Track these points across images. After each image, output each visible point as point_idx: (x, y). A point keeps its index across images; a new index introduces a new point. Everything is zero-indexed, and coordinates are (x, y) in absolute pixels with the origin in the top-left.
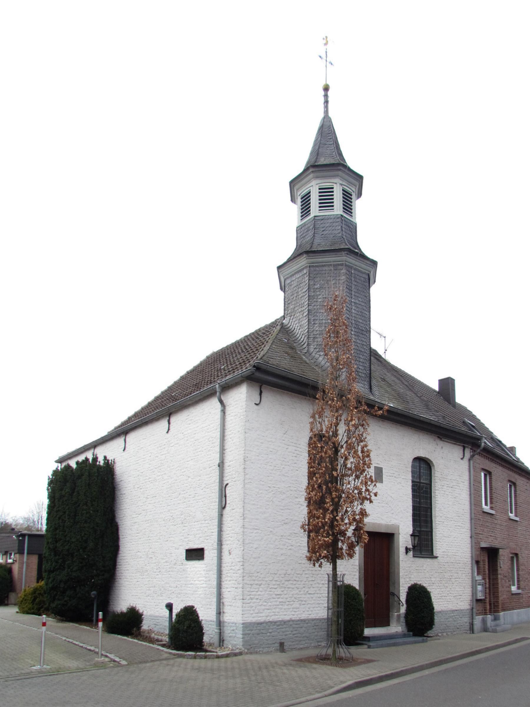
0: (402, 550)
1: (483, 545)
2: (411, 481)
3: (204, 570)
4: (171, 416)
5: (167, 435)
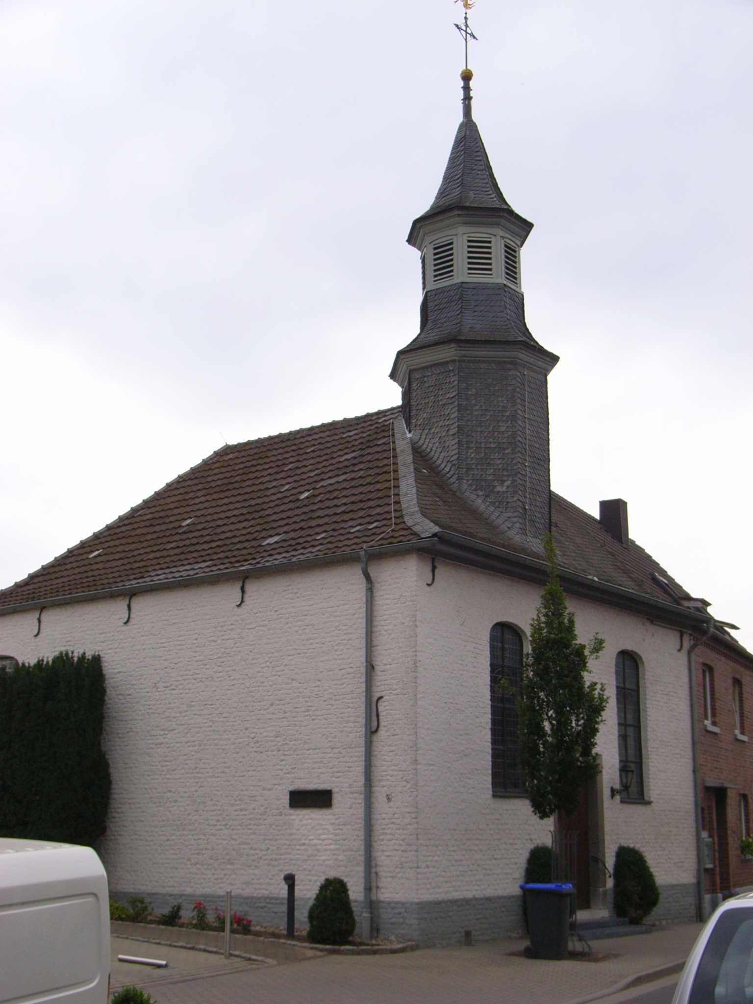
0: (606, 792)
1: (708, 784)
2: (614, 688)
3: (333, 824)
4: (247, 581)
5: (236, 609)
